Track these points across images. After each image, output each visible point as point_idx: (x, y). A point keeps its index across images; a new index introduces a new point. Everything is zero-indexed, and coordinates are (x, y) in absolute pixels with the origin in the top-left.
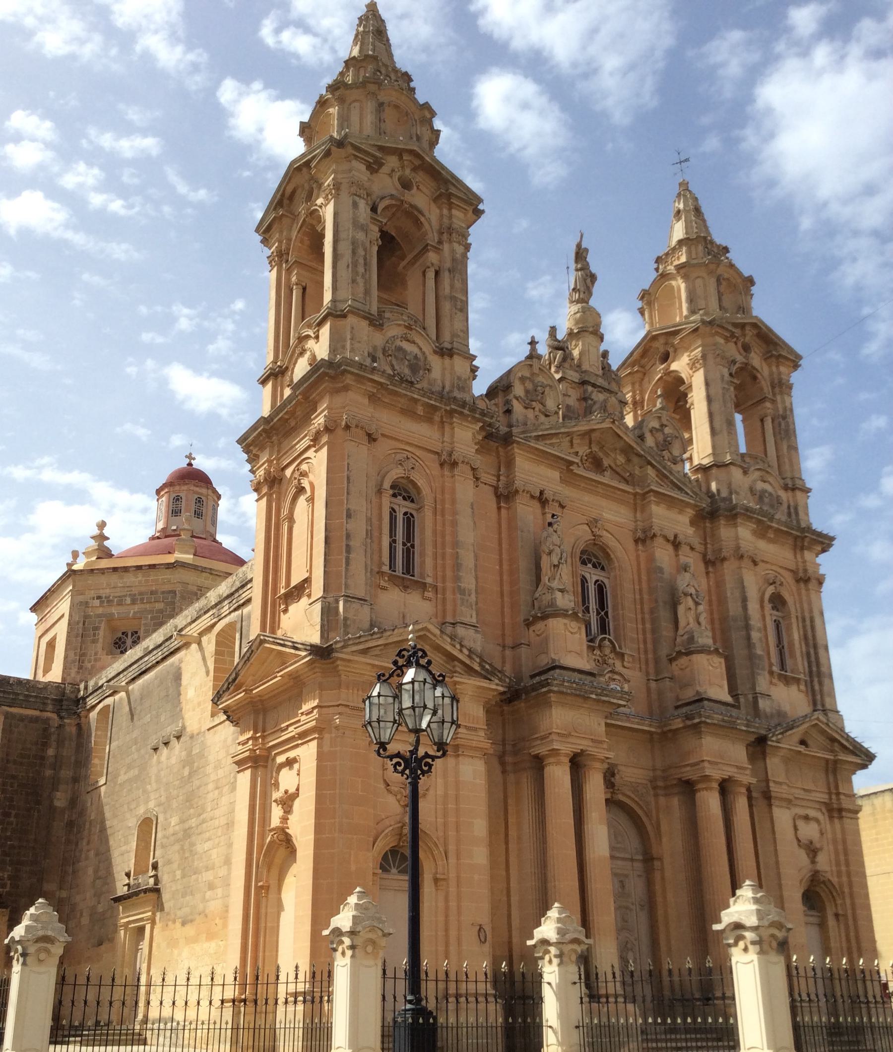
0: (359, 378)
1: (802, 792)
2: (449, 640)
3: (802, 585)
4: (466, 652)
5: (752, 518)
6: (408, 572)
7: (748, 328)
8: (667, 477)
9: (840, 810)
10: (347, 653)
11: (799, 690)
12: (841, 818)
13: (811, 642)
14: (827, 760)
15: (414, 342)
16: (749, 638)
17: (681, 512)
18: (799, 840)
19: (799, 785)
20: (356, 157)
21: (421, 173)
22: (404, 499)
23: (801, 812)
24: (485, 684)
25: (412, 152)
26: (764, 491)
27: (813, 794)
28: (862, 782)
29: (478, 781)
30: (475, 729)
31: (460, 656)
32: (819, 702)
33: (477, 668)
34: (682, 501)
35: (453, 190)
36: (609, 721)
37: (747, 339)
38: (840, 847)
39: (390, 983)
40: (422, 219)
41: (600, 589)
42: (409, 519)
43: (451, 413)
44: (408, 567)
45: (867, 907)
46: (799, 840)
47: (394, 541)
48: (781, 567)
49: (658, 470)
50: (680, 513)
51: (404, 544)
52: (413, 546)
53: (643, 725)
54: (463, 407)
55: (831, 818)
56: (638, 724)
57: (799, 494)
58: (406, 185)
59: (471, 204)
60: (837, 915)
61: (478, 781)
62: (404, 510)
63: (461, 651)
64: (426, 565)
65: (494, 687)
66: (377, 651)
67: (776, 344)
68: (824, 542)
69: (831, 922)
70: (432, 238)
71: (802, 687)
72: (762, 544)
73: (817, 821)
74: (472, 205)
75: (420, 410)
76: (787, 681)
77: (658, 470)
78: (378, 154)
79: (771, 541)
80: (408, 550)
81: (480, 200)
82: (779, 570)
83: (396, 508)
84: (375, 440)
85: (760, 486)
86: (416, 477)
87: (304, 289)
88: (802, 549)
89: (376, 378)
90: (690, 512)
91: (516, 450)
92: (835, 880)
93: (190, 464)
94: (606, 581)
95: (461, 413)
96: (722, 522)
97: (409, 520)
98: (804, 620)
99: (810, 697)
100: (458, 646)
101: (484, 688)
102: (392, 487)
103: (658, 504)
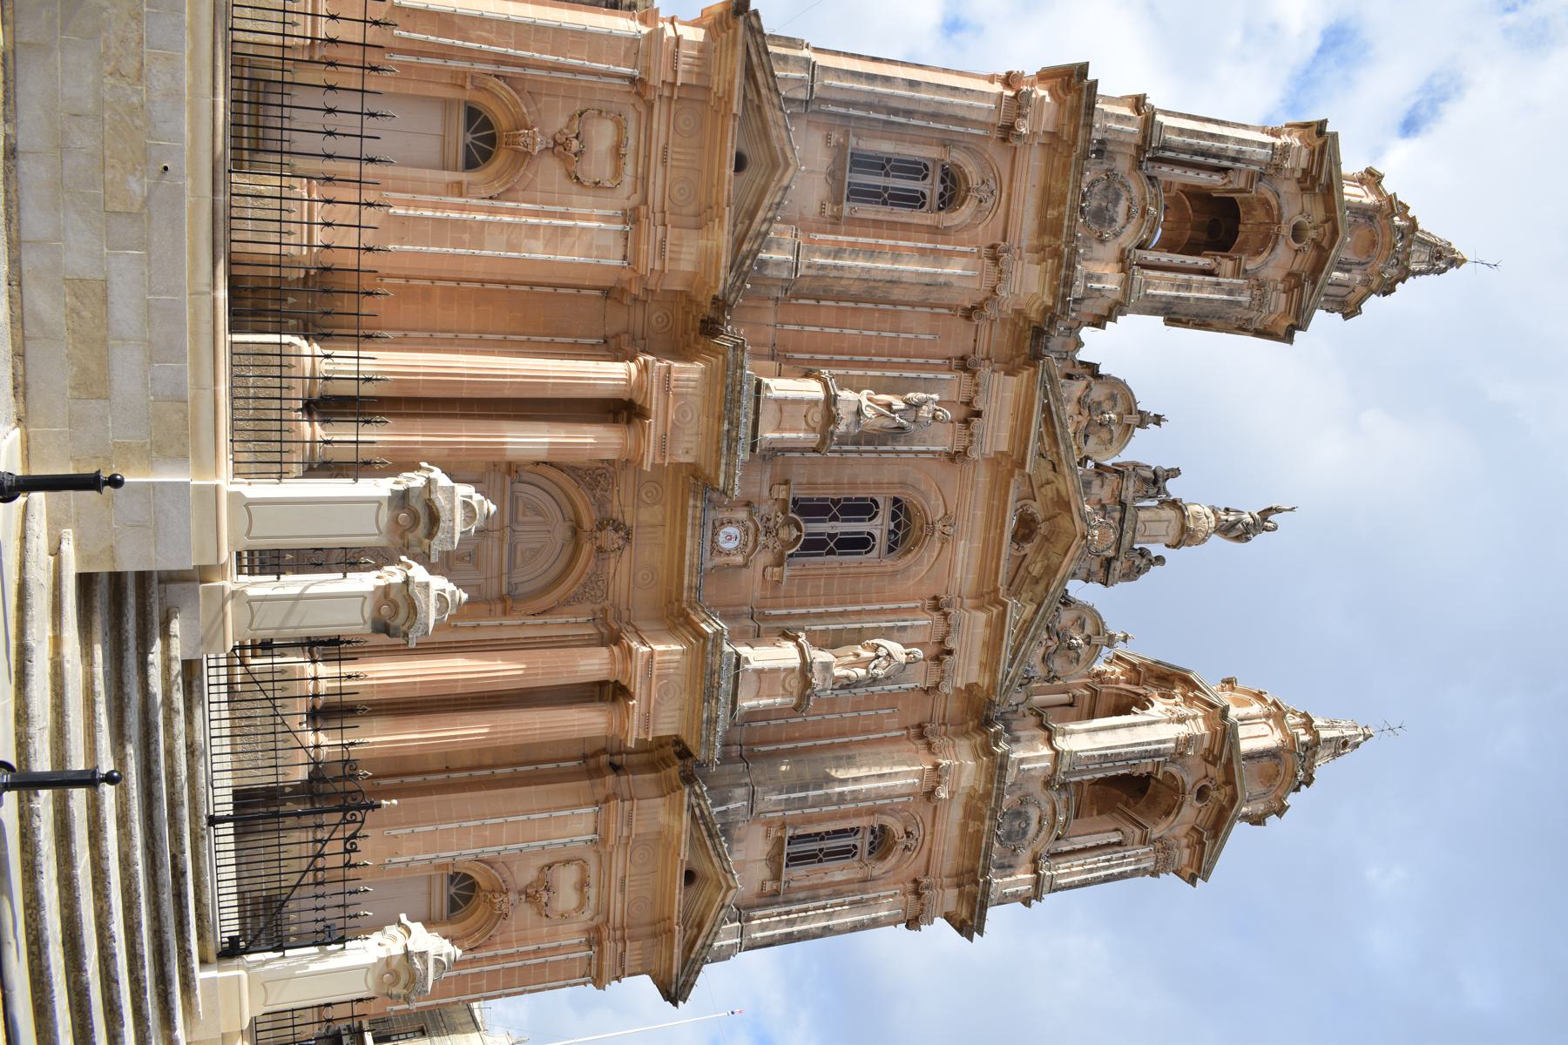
0: (1074, 113)
1: (620, 874)
2: (777, 200)
4: (764, 228)
5: (992, 782)
6: (852, 192)
7: (1228, 789)
8: (1025, 636)
10: (744, 36)
15: (1040, 831)
17: (983, 665)
20: (1312, 153)
21: (1314, 253)
22: (941, 195)
24: (725, 260)
25: (1335, 232)
26: (1027, 820)
27: (660, 169)
30: (629, 824)
31: (755, 225)
33: (745, 247)
34: (998, 662)
35: (1307, 287)
37: (1214, 794)
40: (1265, 254)
42: (848, 852)
43: (1057, 253)
44: (795, 859)
47: (822, 839)
48: (930, 850)
49: (1032, 620)
51: (821, 850)
52: (820, 861)
53: (691, 574)
54: (1068, 268)
56: (691, 566)
58: (1202, 794)
59: (1199, 869)
62: (858, 844)
63: (764, 220)
64: (799, 875)
65: (722, 276)
66: (752, 95)
67: (1216, 836)
68: (969, 924)
70: (1156, 832)
71: (769, 886)
72: (956, 813)
73: (581, 907)
74: (1197, 872)
75: (1052, 213)
76: (774, 861)
77: (1032, 620)
78: (1223, 760)
79: (964, 826)
80: (815, 856)
81: (1205, 879)
83: (859, 835)
84: (929, 799)
85: (1034, 814)
87: (1071, 705)
88: (959, 886)
89: (1081, 132)
90: (985, 681)
91: (1025, 373)
94: (875, 553)
95: (1060, 266)
97: (849, 852)
99: (756, 901)
100: (770, 215)
101: (718, 256)
102: (882, 827)
103: (989, 624)
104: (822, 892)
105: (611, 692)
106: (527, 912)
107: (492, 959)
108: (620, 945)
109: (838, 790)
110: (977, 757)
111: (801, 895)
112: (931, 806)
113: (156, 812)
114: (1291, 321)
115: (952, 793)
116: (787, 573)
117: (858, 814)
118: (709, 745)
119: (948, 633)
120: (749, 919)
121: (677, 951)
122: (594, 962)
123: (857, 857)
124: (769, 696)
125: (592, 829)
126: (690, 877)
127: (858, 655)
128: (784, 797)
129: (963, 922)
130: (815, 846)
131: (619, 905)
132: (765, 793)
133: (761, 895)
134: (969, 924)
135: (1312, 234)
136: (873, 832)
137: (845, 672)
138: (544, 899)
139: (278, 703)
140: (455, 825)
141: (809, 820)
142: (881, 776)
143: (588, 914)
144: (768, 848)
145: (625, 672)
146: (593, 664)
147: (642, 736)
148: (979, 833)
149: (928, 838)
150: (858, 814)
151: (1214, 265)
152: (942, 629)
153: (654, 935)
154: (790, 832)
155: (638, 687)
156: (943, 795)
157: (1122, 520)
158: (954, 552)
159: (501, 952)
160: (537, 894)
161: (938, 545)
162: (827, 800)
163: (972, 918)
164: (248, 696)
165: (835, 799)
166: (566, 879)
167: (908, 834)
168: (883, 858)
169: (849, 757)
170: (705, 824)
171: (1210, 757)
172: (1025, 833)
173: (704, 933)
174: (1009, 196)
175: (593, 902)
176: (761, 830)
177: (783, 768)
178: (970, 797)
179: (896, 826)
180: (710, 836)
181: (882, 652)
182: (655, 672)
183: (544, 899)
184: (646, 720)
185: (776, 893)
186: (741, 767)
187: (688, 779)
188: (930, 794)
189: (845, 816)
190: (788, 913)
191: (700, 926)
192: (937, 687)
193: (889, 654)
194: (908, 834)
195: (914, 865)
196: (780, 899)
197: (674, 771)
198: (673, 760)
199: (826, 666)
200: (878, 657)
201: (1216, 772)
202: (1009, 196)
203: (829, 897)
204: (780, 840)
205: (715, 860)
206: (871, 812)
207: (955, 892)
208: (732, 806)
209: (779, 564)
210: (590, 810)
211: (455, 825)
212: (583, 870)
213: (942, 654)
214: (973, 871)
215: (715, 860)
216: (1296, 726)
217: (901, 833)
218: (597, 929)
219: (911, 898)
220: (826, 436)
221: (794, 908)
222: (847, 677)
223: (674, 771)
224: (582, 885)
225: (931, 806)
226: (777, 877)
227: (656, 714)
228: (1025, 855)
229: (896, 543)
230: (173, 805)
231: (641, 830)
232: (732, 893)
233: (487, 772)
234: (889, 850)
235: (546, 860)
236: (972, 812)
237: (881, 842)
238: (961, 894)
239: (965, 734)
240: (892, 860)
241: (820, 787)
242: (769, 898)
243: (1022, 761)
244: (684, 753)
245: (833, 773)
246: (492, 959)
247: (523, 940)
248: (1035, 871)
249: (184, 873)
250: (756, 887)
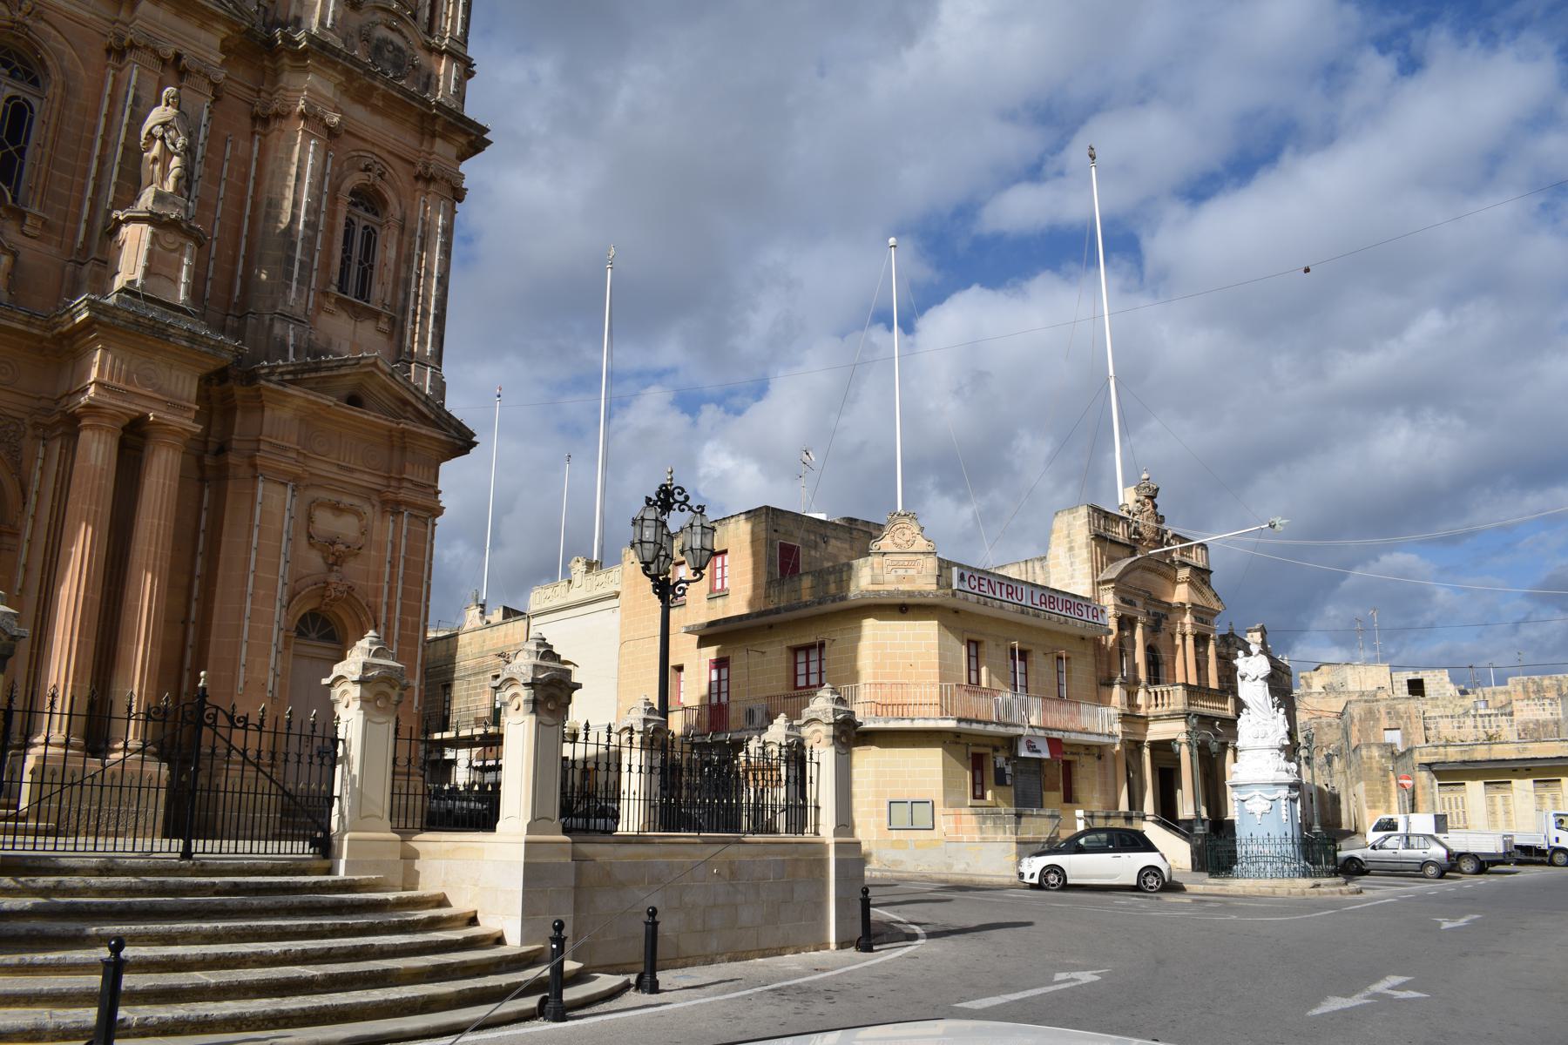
1: (335, 469)
6: (362, 297)
18: (310, 537)
22: (367, 210)
27: (357, 475)
28: (453, 475)
30: (285, 449)
36: (1142, 675)
39: (396, 797)
42: (370, 237)
44: (363, 292)
45: (914, 746)
47: (349, 258)
48: (390, 153)
50: (201, 27)
51: (360, 263)
52: (371, 267)
53: (12, 319)
62: (365, 223)
64: (380, 292)
68: (474, 139)
71: (383, 325)
73: (358, 514)
79: (375, 109)
80: (365, 270)
82: (385, 155)
83: (356, 219)
85: (381, 32)
88: (433, 135)
90: (222, 31)
94: (35, 103)
96: (286, 61)
102: (353, 193)
104: (403, 275)
105: (134, 440)
106: (352, 567)
107: (390, 608)
108: (405, 484)
109: (301, 227)
110: (305, 70)
111: (401, 295)
113: (166, 908)
115: (336, 109)
116: (35, 210)
117: (332, 214)
118: (220, 346)
119: (155, 51)
120: (411, 353)
121: (424, 430)
122: (415, 512)
123: (377, 229)
124: (179, 270)
125: (281, 488)
126: (354, 400)
127: (155, 160)
128: (294, 284)
129: (471, 144)
131: (366, 477)
132: (286, 303)
133: (390, 336)
134: (474, 139)
137: (171, 180)
138: (343, 548)
139: (68, 780)
140: (247, 623)
141: (326, 266)
142: (298, 177)
143: (367, 508)
144: (344, 316)
145: (114, 417)
146: (96, 451)
147: (193, 415)
148: (386, 97)
149: (376, 150)
150: (332, 214)
152: (147, 56)
153: (404, 449)
154: (334, 289)
155: (136, 407)
156: (336, 120)
158: (57, 9)
159: (385, 599)
160: (335, 554)
161: (43, 25)
162: (309, 241)
163: (470, 134)
164: (54, 816)
165: (310, 233)
166: (326, 522)
167: (367, 169)
168: (384, 203)
169: (270, 205)
170: (303, 372)
172: (399, 49)
173: (413, 401)
175: (356, 502)
176: (324, 317)
177: (264, 276)
178: (345, 92)
179: (355, 179)
180: (317, 370)
181: (158, 131)
182: (121, 385)
183: (343, 548)
184: (175, 406)
185: (392, 320)
186: (251, 321)
187: (251, 378)
188: (332, 133)
189: (331, 228)
190: (415, 314)
191: (406, 402)
192: (215, 86)
193: (163, 125)
194: (367, 169)
195: (401, 175)
196: (399, 317)
197: (239, 391)
198: (227, 391)
199: (160, 197)
200: (163, 138)
203: (410, 268)
204: (339, 301)
205: (343, 371)
206: (334, 199)
207: (439, 142)
208: (291, 341)
210: (261, 485)
211: (247, 623)
213: (177, 68)
214: (423, 116)
215: (343, 371)
217: (363, 176)
218: (384, 503)
219: (432, 188)
220: (190, 233)
221: (411, 307)
222: (178, 179)
223: (239, 391)
224: (337, 509)
226: (376, 315)
227: (172, 395)
228: (421, 57)
229: (28, 74)
230: (162, 890)
231: (294, 438)
232: (380, 363)
233: (197, 583)
234: (378, 193)
235: (304, 540)
236: (362, 96)
237: (368, 199)
238: (443, 137)
239: (277, 74)
240: (390, 195)
241: (294, 245)
242: (396, 329)
243: (322, 23)
244: (221, 375)
245: (282, 226)
246: (390, 608)
247: (379, 577)
248: (441, 53)
249: (236, 884)
250: (381, 338)
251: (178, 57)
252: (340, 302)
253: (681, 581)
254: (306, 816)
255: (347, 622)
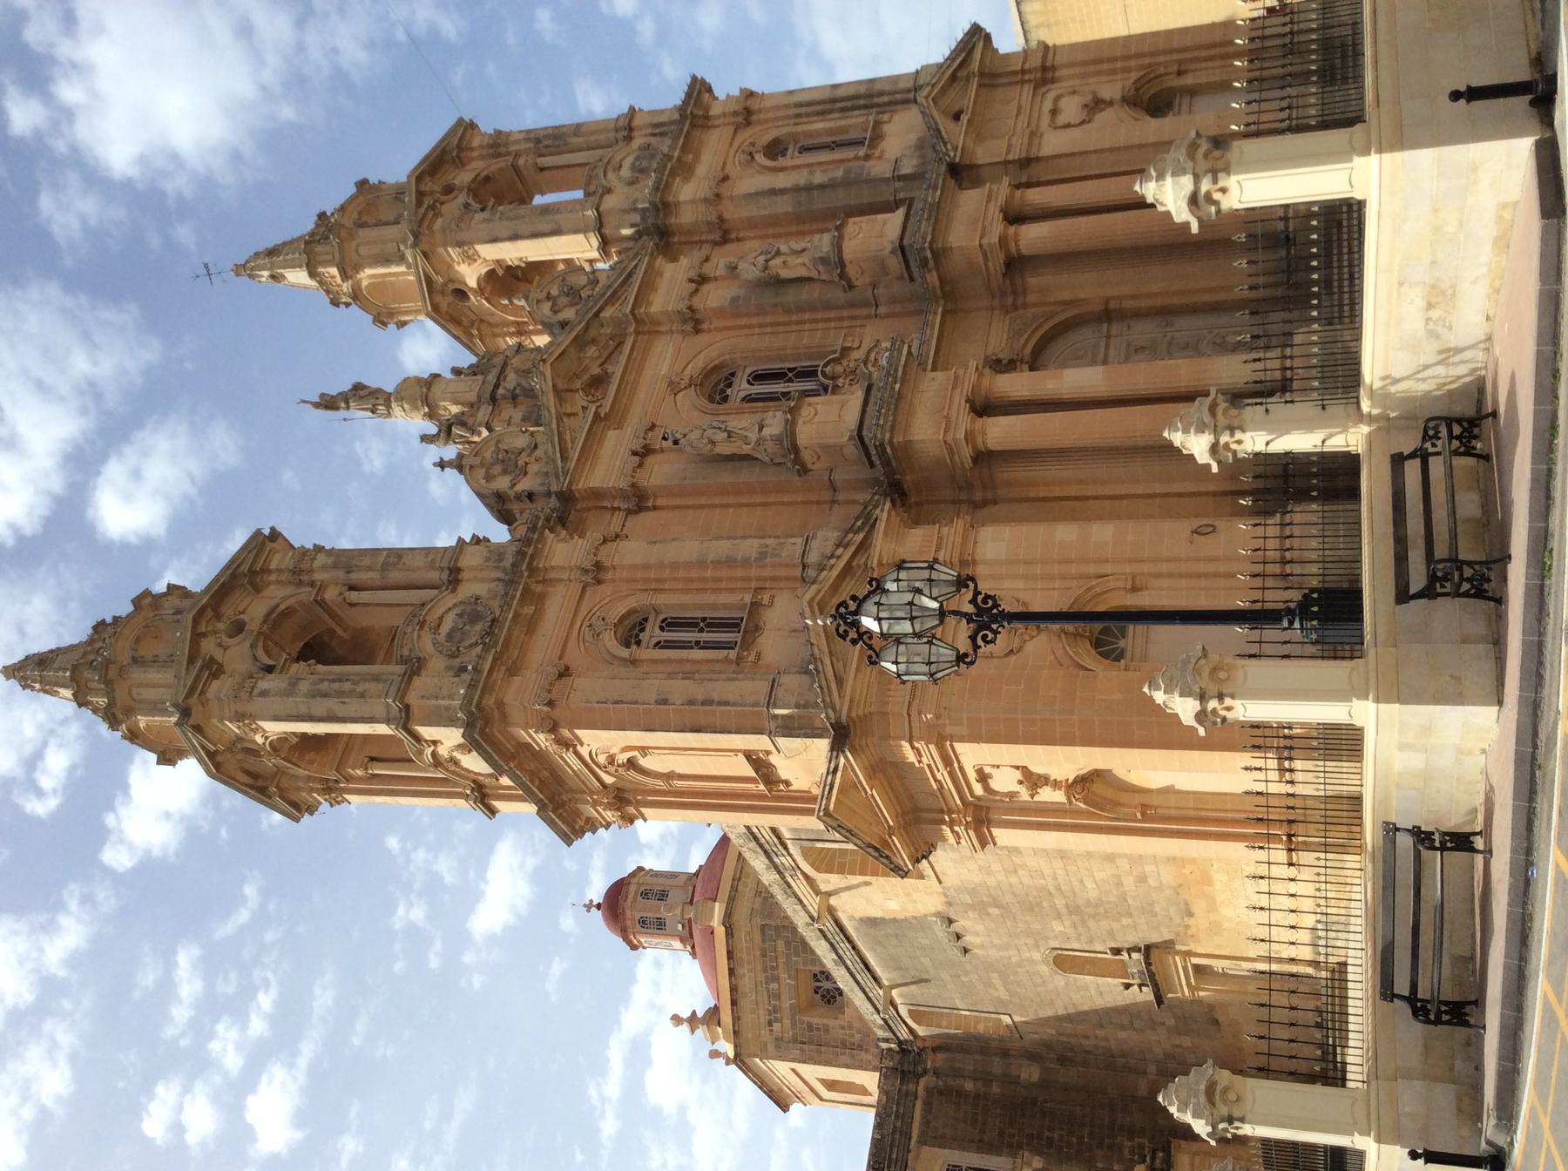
3: (602, 576)
4: (840, 551)
6: (737, 625)
7: (423, 188)
9: (1044, 68)
11: (889, 122)
12: (1054, 68)
13: (828, 106)
14: (980, 86)
15: (441, 618)
16: (822, 187)
17: (660, 274)
18: (1083, 122)
19: (1011, 122)
20: (203, 692)
21: (223, 609)
22: (642, 630)
23: (1046, 118)
24: (881, 526)
25: (196, 621)
26: (633, 167)
27: (1023, 103)
29: (1007, 535)
30: (940, 538)
32: (905, 96)
33: (860, 536)
35: (245, 568)
37: (437, 188)
38: (1092, 68)
40: (282, 607)
41: (758, 377)
42: (670, 624)
43: (532, 570)
44: (731, 625)
46: (1083, 122)
47: (698, 643)
49: (606, 304)
51: (701, 631)
55: (1054, 80)
57: (636, 122)
58: (238, 628)
59: (263, 544)
60: (1180, 73)
61: (1007, 535)
64: (728, 602)
67: (444, 152)
68: (699, 90)
69: (1188, 80)
71: (886, 117)
73: (1057, 99)
75: (528, 610)
76: (756, 630)
77: (606, 304)
78: (199, 664)
79: (697, 159)
80: (709, 625)
81: (258, 533)
83: (654, 640)
86: (614, 616)
87: (372, 759)
88: (707, 117)
90: (660, 261)
92: (1134, 76)
93: (599, 906)
94: (749, 370)
95: (533, 557)
98: (799, 115)
102: (628, 646)
103: (649, 304)
112: (565, 661)
114: (269, 545)
130: (706, 636)
135: (221, 626)
136: (638, 643)
144: (760, 640)
151: (347, 594)
154: (733, 654)
157: (497, 386)
171: (214, 669)
174: (571, 626)
179: (610, 641)
201: (208, 646)
202: (571, 626)
204: (871, 146)
209: (844, 349)
212: (1053, 120)
216: (96, 692)
225: (565, 661)
226: (877, 124)
251: (691, 281)
252: (746, 645)
253: (973, 601)
254: (1333, 478)
255: (1159, 88)
